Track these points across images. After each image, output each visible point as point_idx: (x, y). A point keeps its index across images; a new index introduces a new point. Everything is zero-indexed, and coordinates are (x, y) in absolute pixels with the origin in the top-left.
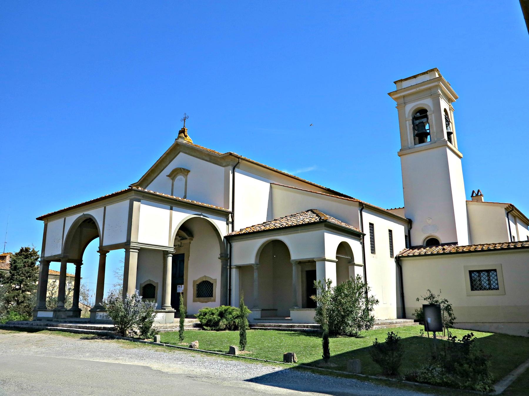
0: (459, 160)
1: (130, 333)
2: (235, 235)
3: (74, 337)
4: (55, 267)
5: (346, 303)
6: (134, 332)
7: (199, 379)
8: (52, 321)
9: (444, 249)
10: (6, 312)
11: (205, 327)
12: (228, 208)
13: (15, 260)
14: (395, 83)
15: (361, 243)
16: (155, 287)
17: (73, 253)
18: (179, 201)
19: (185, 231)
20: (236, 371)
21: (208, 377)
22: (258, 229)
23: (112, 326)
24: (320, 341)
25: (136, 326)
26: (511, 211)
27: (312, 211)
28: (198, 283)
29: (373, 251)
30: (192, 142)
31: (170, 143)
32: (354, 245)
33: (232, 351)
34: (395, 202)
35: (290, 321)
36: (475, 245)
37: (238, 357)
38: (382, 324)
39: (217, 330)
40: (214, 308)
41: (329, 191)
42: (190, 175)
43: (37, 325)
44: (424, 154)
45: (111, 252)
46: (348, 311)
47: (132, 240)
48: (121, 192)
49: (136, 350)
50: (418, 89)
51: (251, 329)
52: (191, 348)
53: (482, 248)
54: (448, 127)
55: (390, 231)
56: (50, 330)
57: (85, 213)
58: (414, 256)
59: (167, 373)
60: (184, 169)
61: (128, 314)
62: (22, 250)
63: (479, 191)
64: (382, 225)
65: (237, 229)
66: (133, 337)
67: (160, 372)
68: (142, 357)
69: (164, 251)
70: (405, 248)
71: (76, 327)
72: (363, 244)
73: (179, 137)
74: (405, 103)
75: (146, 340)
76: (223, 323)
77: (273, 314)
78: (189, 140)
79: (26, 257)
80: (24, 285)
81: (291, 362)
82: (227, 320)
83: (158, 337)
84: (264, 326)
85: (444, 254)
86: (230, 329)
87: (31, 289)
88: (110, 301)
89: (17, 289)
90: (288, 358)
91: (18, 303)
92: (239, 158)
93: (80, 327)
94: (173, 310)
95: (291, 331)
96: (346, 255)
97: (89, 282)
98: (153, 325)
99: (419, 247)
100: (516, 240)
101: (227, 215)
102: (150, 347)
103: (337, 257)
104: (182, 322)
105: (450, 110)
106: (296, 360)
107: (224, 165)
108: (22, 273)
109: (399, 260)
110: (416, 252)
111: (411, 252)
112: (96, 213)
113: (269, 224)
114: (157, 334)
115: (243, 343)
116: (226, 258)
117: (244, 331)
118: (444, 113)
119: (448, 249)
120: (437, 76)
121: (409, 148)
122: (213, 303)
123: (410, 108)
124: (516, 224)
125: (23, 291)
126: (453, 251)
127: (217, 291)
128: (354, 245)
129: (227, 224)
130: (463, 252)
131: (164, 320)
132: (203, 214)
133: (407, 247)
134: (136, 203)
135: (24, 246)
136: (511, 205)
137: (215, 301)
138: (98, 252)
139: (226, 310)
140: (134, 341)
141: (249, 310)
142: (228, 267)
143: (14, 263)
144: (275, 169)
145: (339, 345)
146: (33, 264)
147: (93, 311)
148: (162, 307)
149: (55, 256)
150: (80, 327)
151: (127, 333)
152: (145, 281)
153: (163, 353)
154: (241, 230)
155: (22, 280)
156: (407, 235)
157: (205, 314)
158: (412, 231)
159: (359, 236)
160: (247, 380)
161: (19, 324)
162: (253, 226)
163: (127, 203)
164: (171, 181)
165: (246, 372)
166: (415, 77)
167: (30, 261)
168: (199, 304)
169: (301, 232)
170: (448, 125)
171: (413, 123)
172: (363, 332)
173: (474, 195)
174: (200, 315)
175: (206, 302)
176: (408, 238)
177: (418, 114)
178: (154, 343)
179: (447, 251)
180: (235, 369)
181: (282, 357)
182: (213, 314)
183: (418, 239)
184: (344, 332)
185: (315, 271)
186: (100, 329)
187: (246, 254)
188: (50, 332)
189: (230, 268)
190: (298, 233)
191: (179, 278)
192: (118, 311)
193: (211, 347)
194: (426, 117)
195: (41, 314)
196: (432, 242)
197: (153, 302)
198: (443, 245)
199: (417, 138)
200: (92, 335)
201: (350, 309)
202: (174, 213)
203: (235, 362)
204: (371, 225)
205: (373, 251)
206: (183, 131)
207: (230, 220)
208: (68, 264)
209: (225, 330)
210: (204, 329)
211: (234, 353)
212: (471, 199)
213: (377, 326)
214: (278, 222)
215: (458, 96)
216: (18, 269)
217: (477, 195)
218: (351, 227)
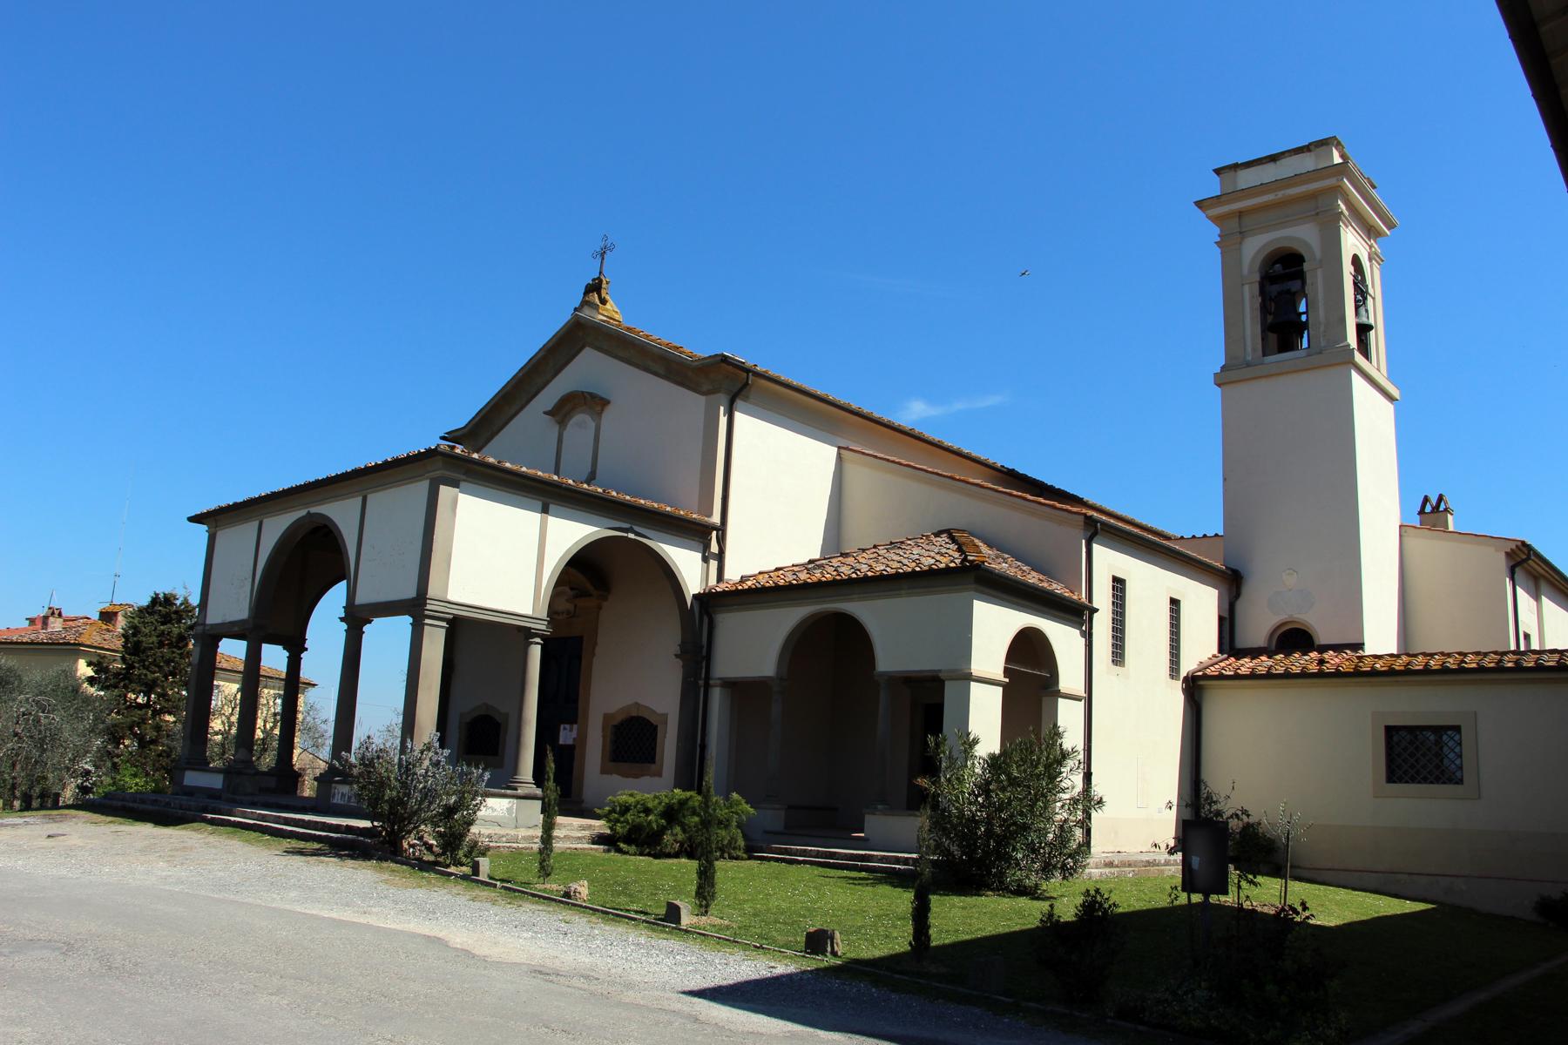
0: (1389, 408)
1: (413, 846)
2: (724, 594)
3: (267, 845)
4: (232, 650)
5: (1009, 803)
6: (426, 844)
7: (562, 980)
8: (219, 798)
9: (1321, 662)
10: (109, 764)
12: (710, 515)
13: (134, 627)
14: (1218, 171)
15: (1083, 634)
16: (498, 725)
17: (280, 613)
18: (569, 489)
19: (584, 575)
20: (663, 968)
21: (587, 977)
22: (790, 578)
23: (366, 824)
24: (904, 900)
25: (429, 829)
26: (1524, 561)
27: (949, 532)
28: (616, 722)
29: (1118, 656)
32: (1063, 638)
33: (673, 914)
34: (1196, 514)
35: (863, 843)
36: (1408, 655)
37: (686, 931)
38: (1124, 864)
39: (656, 856)
40: (650, 796)
41: (1013, 478)
42: (608, 415)
44: (1286, 388)
45: (378, 622)
46: (1015, 823)
47: (431, 592)
49: (420, 894)
50: (1280, 194)
51: (750, 858)
52: (567, 899)
53: (1427, 664)
54: (1362, 310)
55: (1175, 603)
56: (212, 822)
57: (313, 510)
58: (1237, 677)
59: (484, 959)
61: (408, 795)
62: (155, 600)
63: (1441, 498)
64: (1151, 584)
65: (733, 573)
66: (419, 859)
67: (468, 954)
68: (430, 913)
69: (520, 628)
70: (1215, 652)
71: (278, 820)
72: (1088, 636)
74: (1243, 234)
75: (452, 869)
76: (671, 839)
77: (813, 819)
78: (612, 311)
79: (166, 619)
80: (159, 695)
81: (824, 953)
82: (684, 831)
83: (485, 863)
85: (1321, 675)
87: (177, 707)
88: (363, 758)
89: (140, 706)
90: (817, 942)
91: (143, 743)
92: (747, 371)
93: (287, 822)
94: (539, 792)
95: (861, 869)
96: (1038, 666)
97: (319, 703)
98: (474, 829)
99: (1254, 653)
100: (1535, 646)
101: (704, 534)
102: (460, 888)
103: (1007, 672)
104: (548, 827)
105: (1370, 259)
106: (840, 950)
107: (705, 388)
108: (154, 663)
109: (1195, 688)
110: (1246, 666)
111: (1230, 665)
112: (341, 513)
113: (821, 566)
114: (484, 855)
115: (705, 894)
116: (696, 654)
117: (711, 864)
118: (1352, 269)
119: (1333, 660)
120: (1337, 160)
121: (1248, 365)
122: (656, 779)
123: (1255, 247)
124: (1537, 598)
125: (156, 713)
126: (1347, 667)
128: (1063, 638)
129: (705, 560)
130: (1374, 673)
131: (503, 818)
132: (636, 528)
133: (1221, 651)
135: (163, 589)
136: (1523, 543)
137: (659, 774)
139: (683, 803)
140: (421, 869)
141: (748, 807)
142: (701, 683)
143: (134, 635)
144: (854, 406)
145: (962, 918)
146: (182, 639)
147: (324, 780)
148: (504, 783)
149: (231, 623)
150: (287, 822)
151: (405, 845)
152: (465, 705)
153: (488, 905)
154: (743, 579)
155: (155, 681)
156: (1226, 615)
157: (626, 809)
158: (1241, 606)
159: (1077, 614)
160: (684, 993)
161: (143, 802)
162: (778, 569)
163: (423, 486)
164: (556, 428)
165: (696, 971)
166: (1273, 158)
167: (176, 631)
168: (616, 779)
169: (909, 595)
170: (1360, 303)
171: (1262, 292)
172: (1054, 885)
173: (1428, 509)
174: (610, 812)
175: (636, 776)
176: (1227, 625)
178: (472, 878)
179: (1327, 668)
180: (669, 961)
181: (802, 939)
182: (647, 811)
183: (1258, 626)
184: (1002, 882)
186: (337, 828)
187: (752, 650)
188: (210, 828)
189: (707, 686)
190: (900, 596)
191: (561, 701)
192: (383, 784)
193: (623, 899)
194: (1300, 276)
195: (192, 778)
196: (1294, 639)
197: (477, 767)
198: (1323, 649)
199: (1273, 337)
200: (316, 846)
201: (1020, 820)
203: (674, 943)
204: (1119, 584)
205: (1118, 656)
206: (595, 287)
207: (714, 548)
208: (265, 646)
209: (677, 855)
210: (619, 851)
211: (678, 921)
212: (1416, 520)
213: (1107, 870)
214: (850, 560)
215: (1395, 220)
216: (144, 651)
217: (1436, 509)
218: (1058, 588)
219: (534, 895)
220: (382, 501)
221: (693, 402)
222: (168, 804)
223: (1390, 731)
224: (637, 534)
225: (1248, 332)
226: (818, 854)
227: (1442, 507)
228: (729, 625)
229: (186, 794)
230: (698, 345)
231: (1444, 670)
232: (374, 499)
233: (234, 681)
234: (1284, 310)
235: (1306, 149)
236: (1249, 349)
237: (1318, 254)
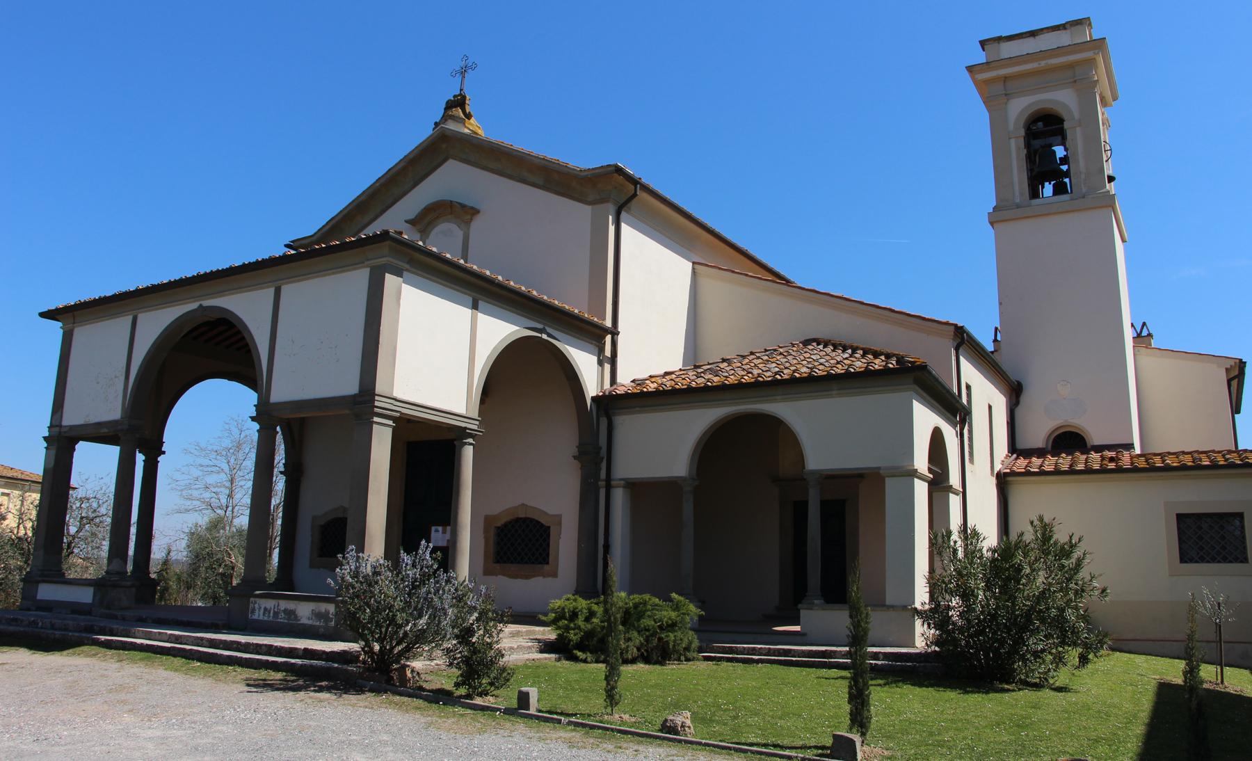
8: (89, 613)
11: (579, 654)
12: (604, 319)
18: (500, 286)
28: (499, 524)
30: (480, 132)
31: (422, 132)
42: (477, 224)
43: (53, 627)
44: (1055, 228)
47: (379, 388)
48: (170, 282)
50: (1043, 63)
56: (108, 645)
57: (207, 303)
58: (1028, 473)
60: (463, 206)
65: (627, 375)
73: (446, 118)
74: (1008, 96)
84: (731, 651)
86: (647, 661)
93: (200, 642)
99: (1040, 453)
101: (598, 335)
111: (1022, 463)
112: (249, 308)
116: (594, 456)
121: (1018, 207)
123: (1019, 107)
127: (566, 547)
129: (600, 363)
132: (549, 330)
134: (390, 279)
137: (555, 575)
138: (45, 438)
142: (602, 483)
158: (1019, 412)
162: (667, 374)
166: (1033, 34)
168: (502, 581)
171: (1028, 145)
175: (527, 577)
177: (1040, 124)
183: (1037, 433)
185: (806, 503)
187: (661, 451)
189: (609, 487)
190: (831, 396)
196: (1068, 441)
198: (1099, 449)
202: (482, 318)
205: (972, 460)
206: (459, 102)
210: (575, 659)
219: (687, 742)
220: (303, 295)
221: (578, 214)
222: (35, 623)
223: (1180, 517)
224: (549, 335)
225: (1016, 179)
226: (769, 652)
227: (1145, 333)
228: (629, 427)
229: (38, 609)
230: (582, 156)
231: (1183, 468)
232: (288, 290)
233: (34, 491)
234: (1046, 157)
235: (1062, 27)
236: (1017, 194)
237: (1076, 115)
